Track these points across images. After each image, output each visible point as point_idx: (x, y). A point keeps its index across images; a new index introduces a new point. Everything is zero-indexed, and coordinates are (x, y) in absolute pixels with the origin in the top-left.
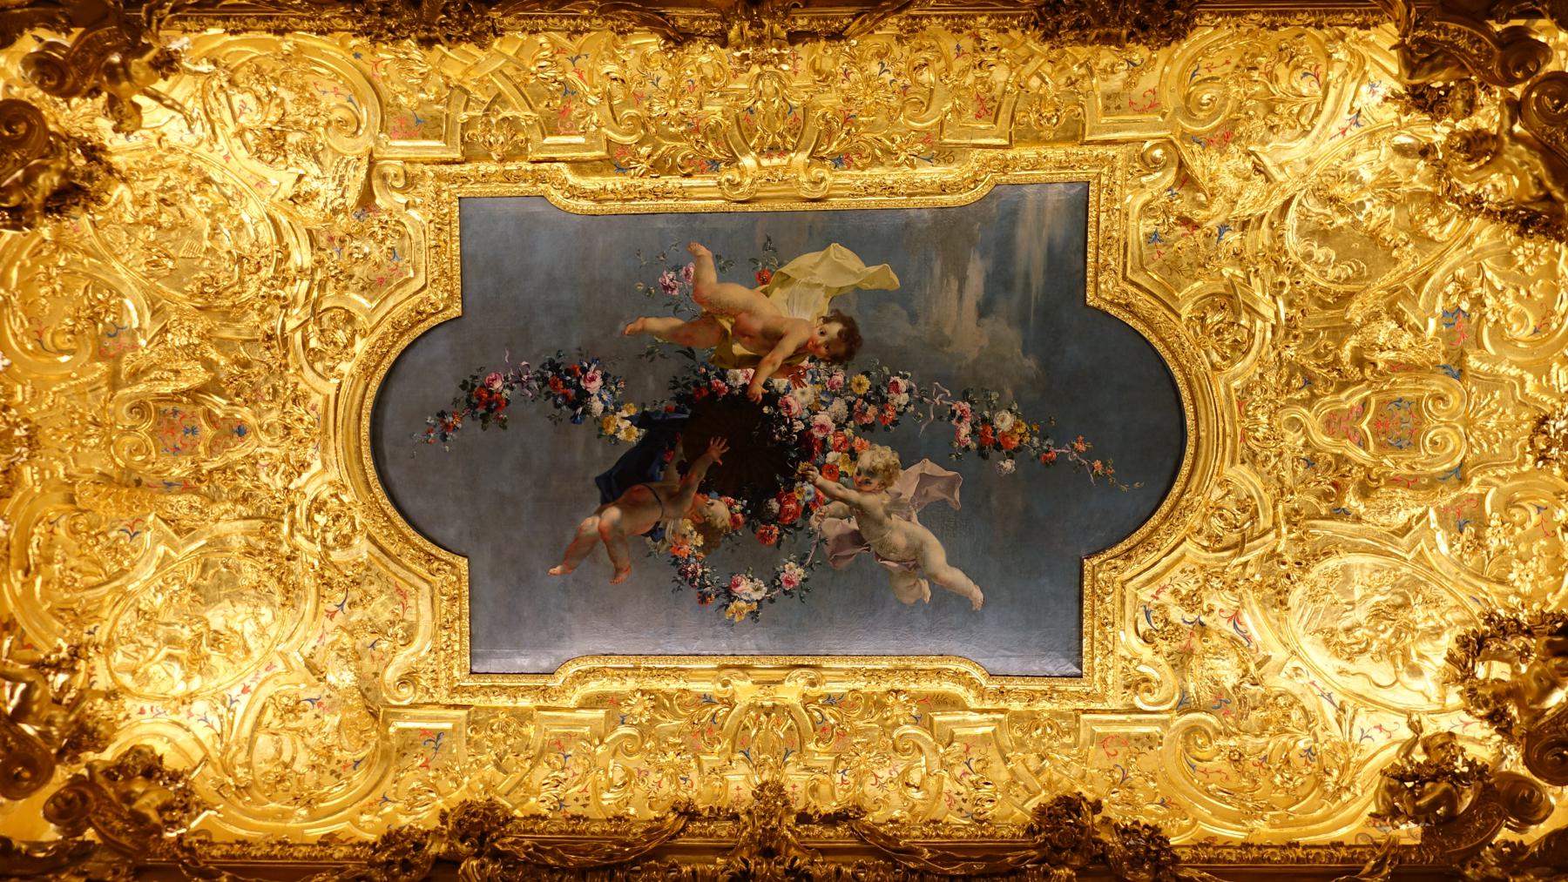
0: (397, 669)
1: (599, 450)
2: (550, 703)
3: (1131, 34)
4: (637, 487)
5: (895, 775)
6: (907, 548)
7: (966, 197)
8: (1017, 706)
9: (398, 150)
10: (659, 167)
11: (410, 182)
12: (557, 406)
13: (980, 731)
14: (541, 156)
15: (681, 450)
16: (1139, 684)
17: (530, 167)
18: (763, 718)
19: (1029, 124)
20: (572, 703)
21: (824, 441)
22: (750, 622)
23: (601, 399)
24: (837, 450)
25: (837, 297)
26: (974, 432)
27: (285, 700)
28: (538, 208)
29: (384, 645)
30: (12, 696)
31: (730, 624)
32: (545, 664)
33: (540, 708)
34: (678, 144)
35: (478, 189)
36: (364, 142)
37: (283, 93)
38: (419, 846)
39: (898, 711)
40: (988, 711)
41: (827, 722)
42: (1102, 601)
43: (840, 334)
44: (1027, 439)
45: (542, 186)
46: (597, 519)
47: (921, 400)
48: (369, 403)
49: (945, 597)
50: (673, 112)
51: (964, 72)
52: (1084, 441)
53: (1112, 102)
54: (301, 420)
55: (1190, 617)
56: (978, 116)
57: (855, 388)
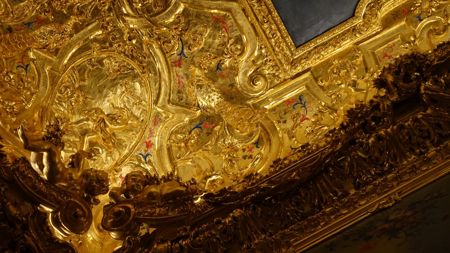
30: (41, 167)
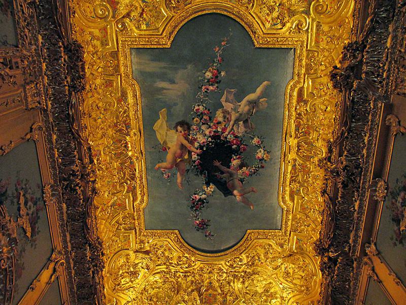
0: (278, 248)
2: (291, 210)
3: (81, 61)
5: (322, 113)
6: (249, 106)
7: (137, 88)
8: (303, 71)
9: (134, 245)
10: (133, 178)
11: (142, 242)
12: (204, 207)
14: (132, 210)
15: (217, 174)
16: (299, 28)
19: (113, 69)
20: (292, 204)
25: (169, 128)
26: (212, 85)
28: (147, 210)
31: (271, 159)
32: (280, 211)
33: (293, 212)
34: (127, 173)
35: (142, 225)
36: (131, 253)
37: (121, 272)
38: (325, 263)
39: (302, 109)
40: (304, 80)
41: (303, 131)
45: (141, 209)
47: (202, 102)
48: (203, 254)
49: (264, 94)
50: (117, 176)
51: (99, 94)
53: (104, 44)
54: (207, 269)
55: (277, 9)
57: (198, 122)
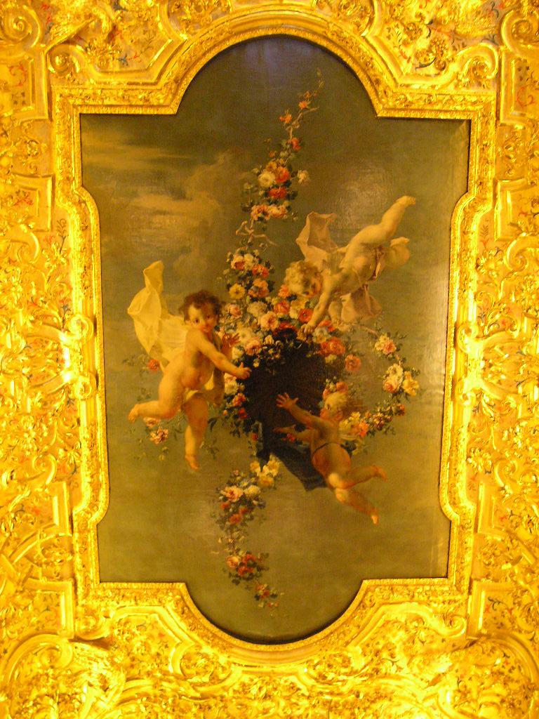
1: (286, 489)
2: (472, 524)
4: (314, 460)
10: (70, 445)
11: (91, 612)
13: (509, 201)
14: (68, 525)
15: (286, 429)
16: (476, 72)
17: (76, 535)
18: (493, 369)
21: (281, 320)
22: (420, 377)
23: (247, 487)
24: (287, 310)
26: (276, 203)
27: (457, 699)
29: (423, 634)
33: (476, 530)
37: (35, 693)
40: (495, 195)
42: (411, 103)
43: (198, 307)
44: (281, 161)
46: (338, 490)
47: (250, 244)
49: (405, 226)
52: (284, 115)
55: (426, 32)
56: (30, 203)
